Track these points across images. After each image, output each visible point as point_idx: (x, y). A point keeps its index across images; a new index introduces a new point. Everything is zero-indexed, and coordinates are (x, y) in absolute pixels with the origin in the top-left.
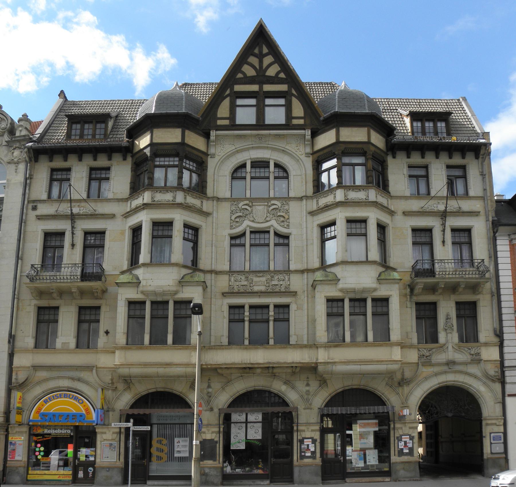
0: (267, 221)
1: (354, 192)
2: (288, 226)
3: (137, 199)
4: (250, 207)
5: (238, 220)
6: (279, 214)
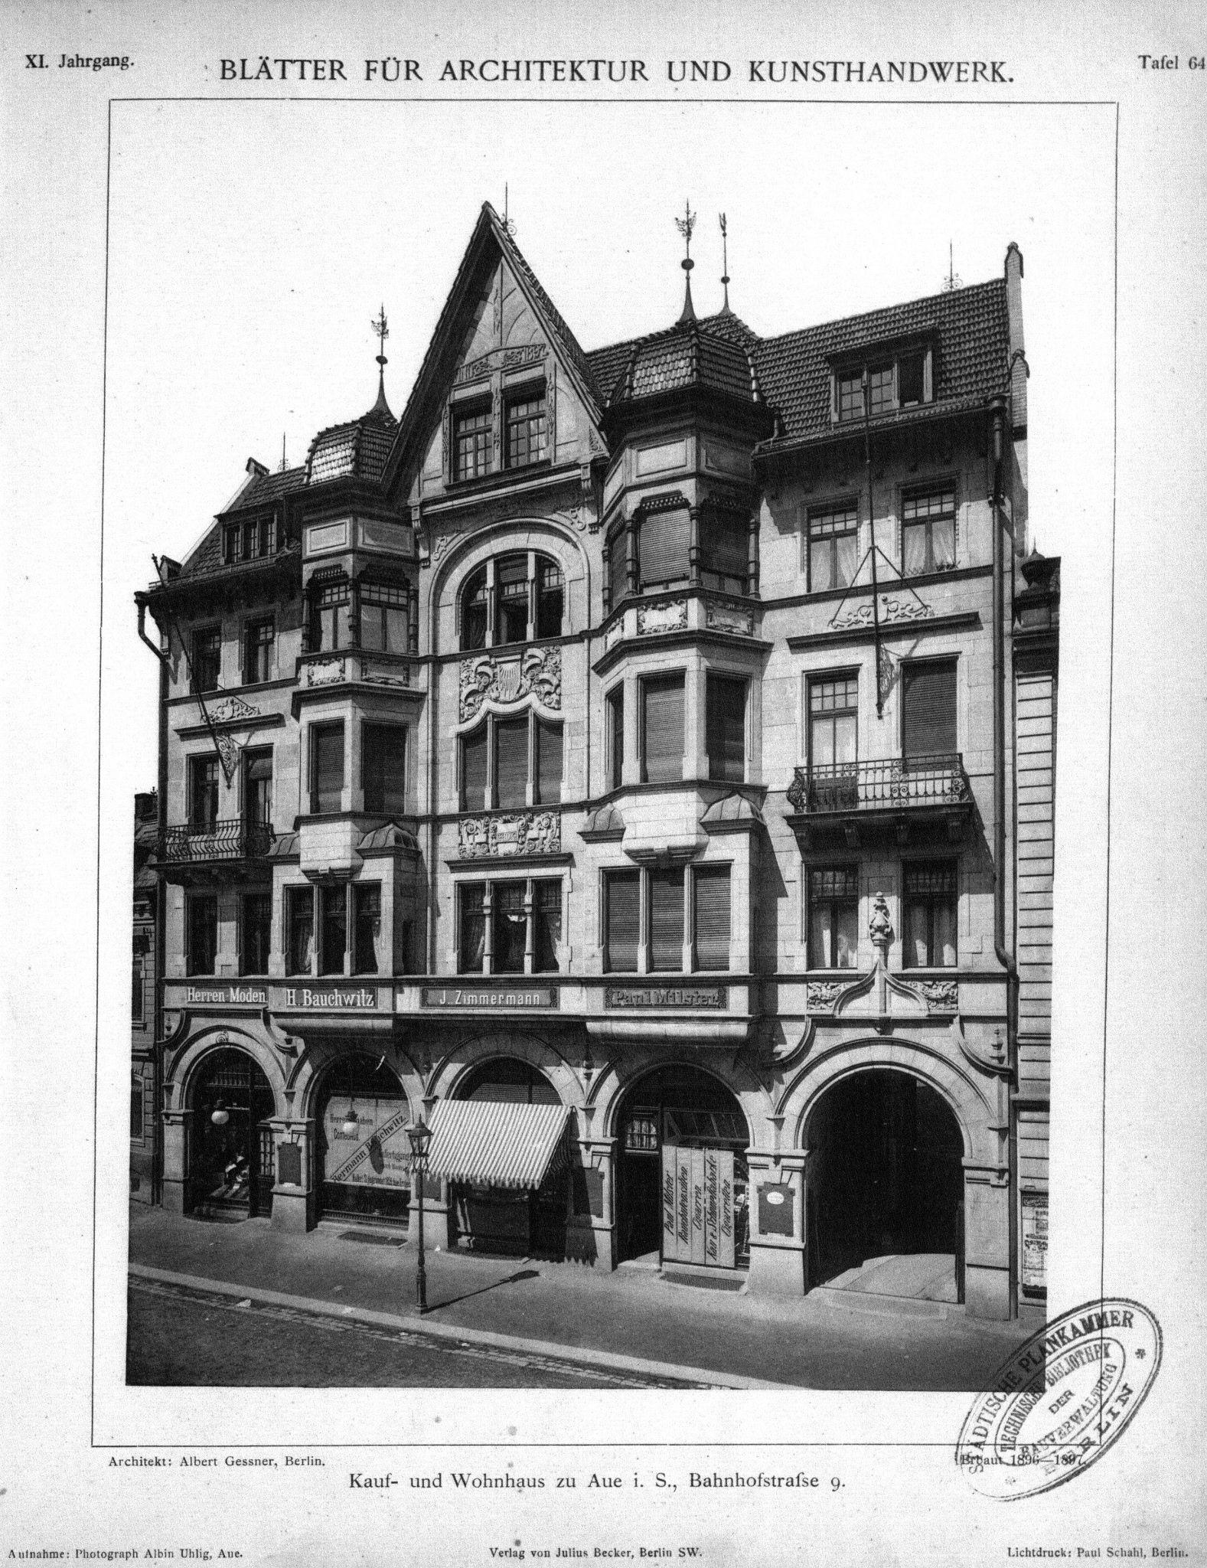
0: (522, 697)
1: (656, 612)
2: (559, 702)
3: (660, 609)
4: (493, 667)
5: (470, 700)
6: (542, 676)
